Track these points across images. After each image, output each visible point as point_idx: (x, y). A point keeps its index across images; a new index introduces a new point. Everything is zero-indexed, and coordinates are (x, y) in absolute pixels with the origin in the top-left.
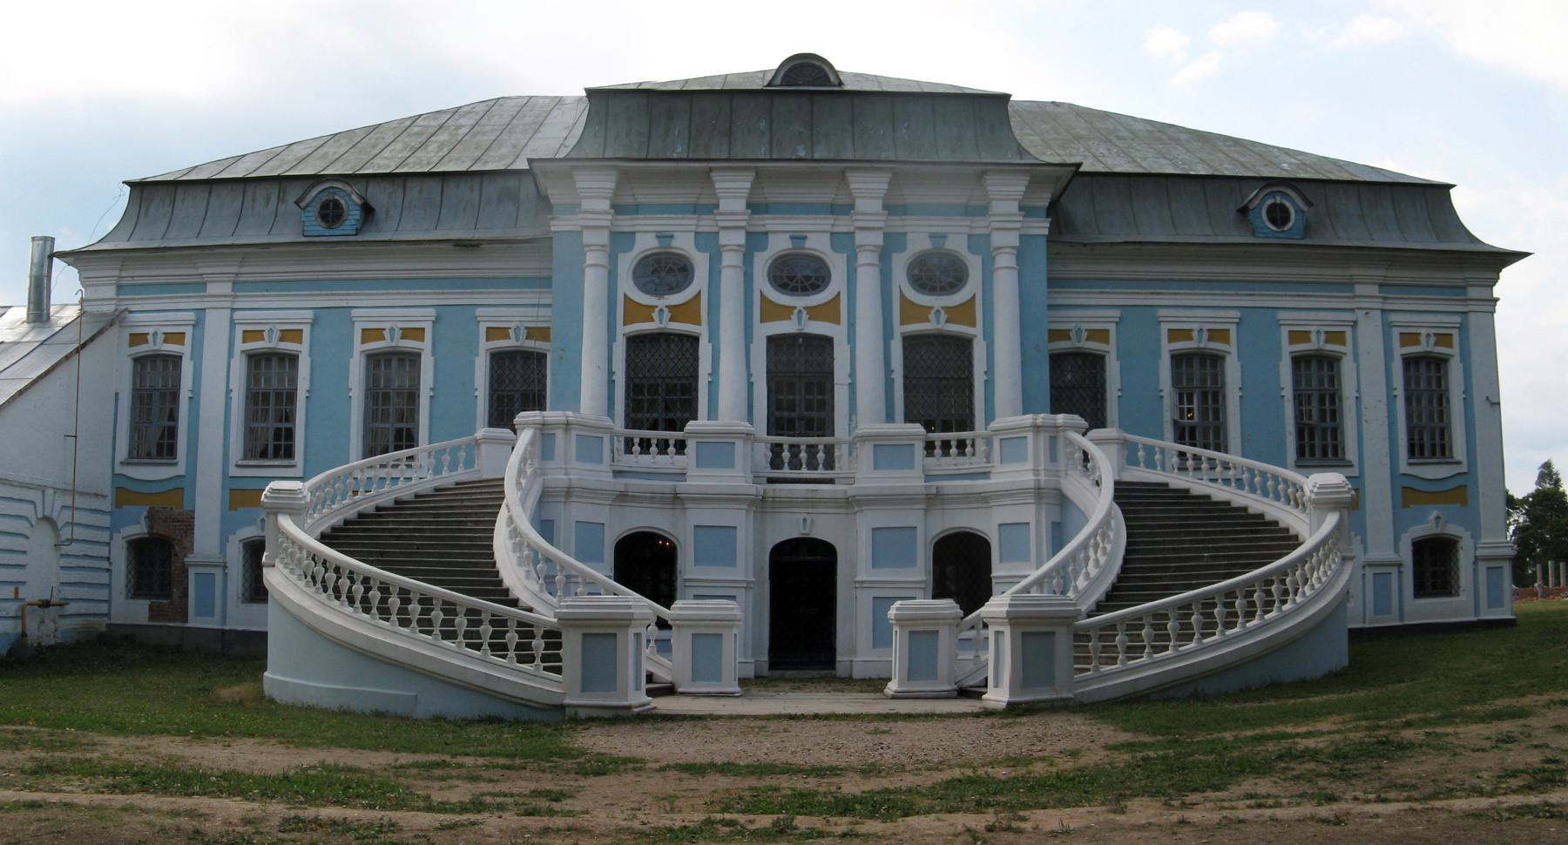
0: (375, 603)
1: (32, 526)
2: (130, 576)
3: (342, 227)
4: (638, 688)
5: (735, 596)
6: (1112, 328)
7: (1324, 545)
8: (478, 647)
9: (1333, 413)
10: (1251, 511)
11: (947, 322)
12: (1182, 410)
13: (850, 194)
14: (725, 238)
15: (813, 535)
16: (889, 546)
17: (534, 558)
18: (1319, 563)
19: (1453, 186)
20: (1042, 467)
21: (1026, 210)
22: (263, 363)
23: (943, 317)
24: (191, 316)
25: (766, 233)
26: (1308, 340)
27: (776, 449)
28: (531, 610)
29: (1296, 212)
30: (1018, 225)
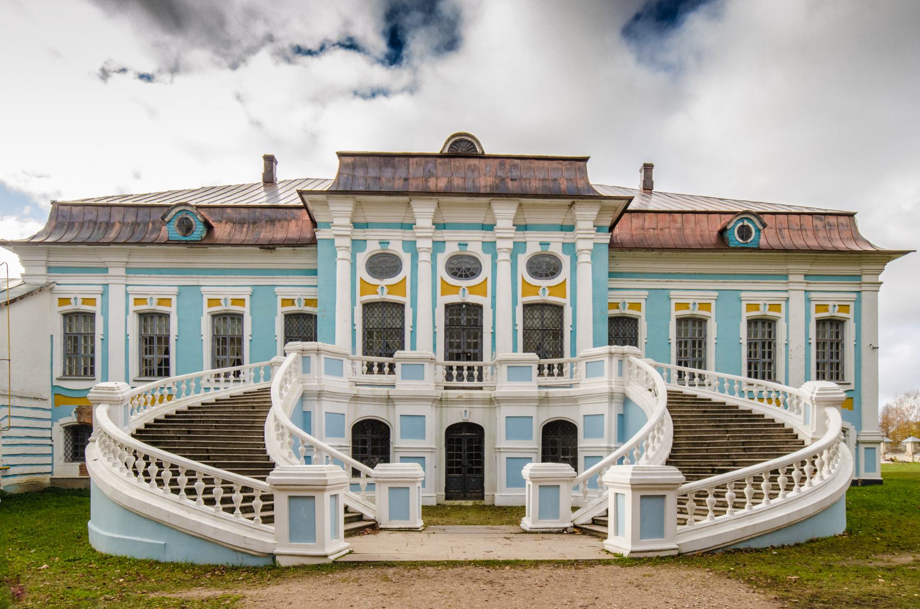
3: (193, 236)
6: (643, 302)
7: (829, 449)
8: (232, 511)
9: (770, 353)
11: (549, 295)
14: (420, 244)
16: (517, 427)
17: (295, 443)
20: (613, 380)
22: (149, 320)
23: (547, 292)
24: (100, 288)
25: (444, 242)
26: (758, 309)
29: (756, 231)
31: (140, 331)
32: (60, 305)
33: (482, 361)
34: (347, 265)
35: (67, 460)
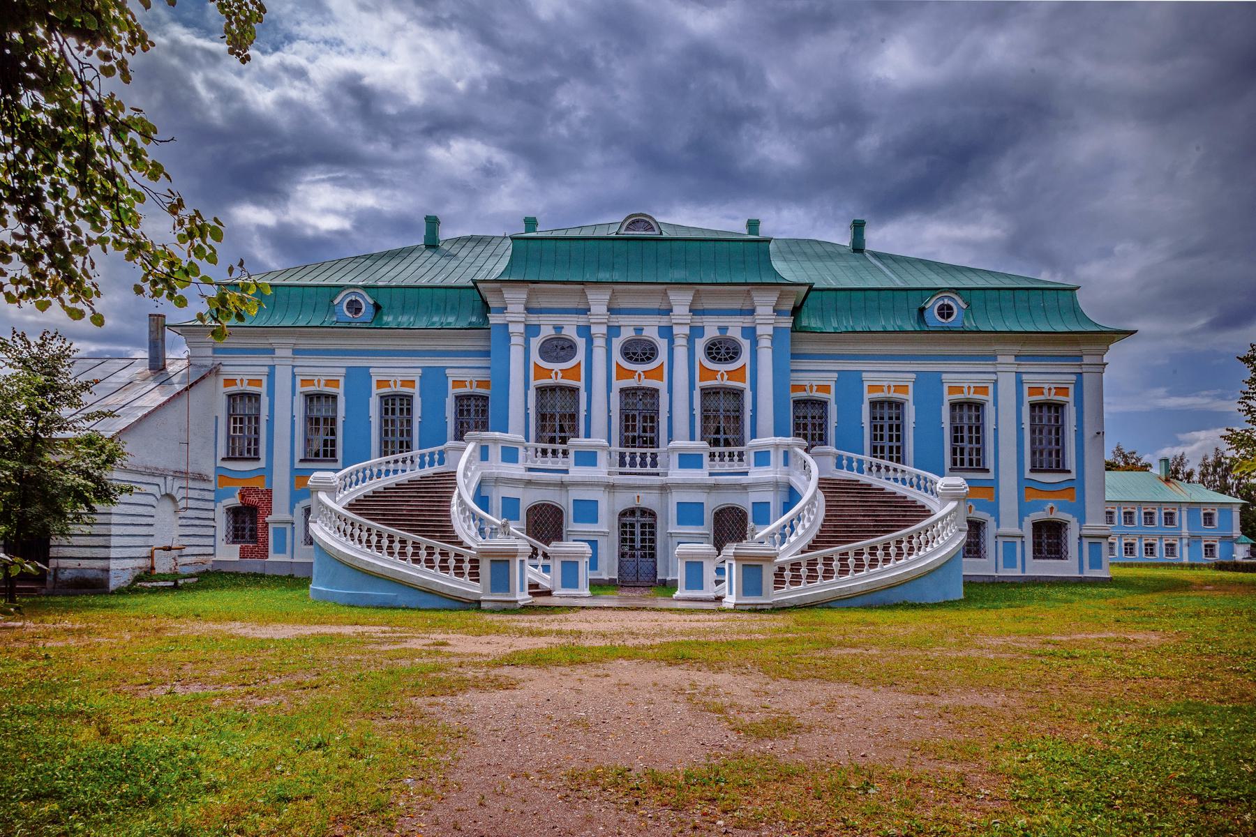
2: (1064, 547)
4: (522, 590)
5: (487, 459)
13: (670, 303)
21: (777, 311)
25: (620, 327)
27: (622, 456)
28: (470, 548)
30: (773, 321)
31: (306, 412)
32: (226, 386)
34: (521, 349)
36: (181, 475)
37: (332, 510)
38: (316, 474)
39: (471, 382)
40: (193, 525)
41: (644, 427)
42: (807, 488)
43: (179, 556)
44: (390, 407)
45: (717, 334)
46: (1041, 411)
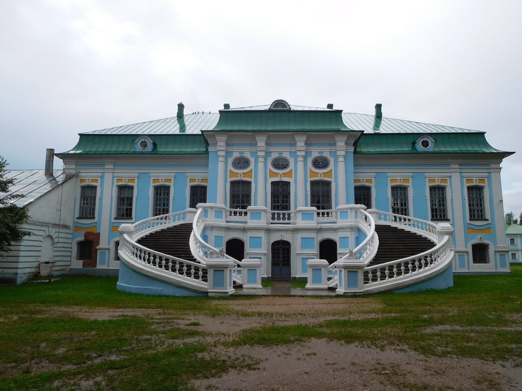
0: (151, 261)
1: (44, 238)
4: (230, 286)
9: (157, 200)
10: (398, 228)
12: (394, 204)
13: (295, 141)
15: (284, 239)
18: (443, 251)
19: (485, 133)
26: (435, 182)
27: (273, 214)
28: (199, 263)
30: (345, 149)
33: (290, 210)
35: (78, 259)
36: (56, 226)
37: (130, 243)
38: (123, 225)
39: (198, 179)
40: (60, 251)
41: (282, 200)
42: (370, 231)
43: (53, 266)
44: (159, 192)
45: (318, 155)
46: (472, 191)
